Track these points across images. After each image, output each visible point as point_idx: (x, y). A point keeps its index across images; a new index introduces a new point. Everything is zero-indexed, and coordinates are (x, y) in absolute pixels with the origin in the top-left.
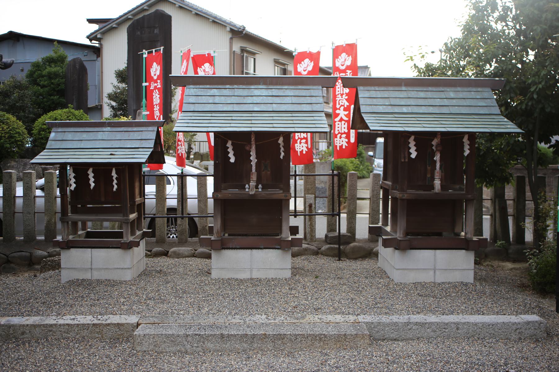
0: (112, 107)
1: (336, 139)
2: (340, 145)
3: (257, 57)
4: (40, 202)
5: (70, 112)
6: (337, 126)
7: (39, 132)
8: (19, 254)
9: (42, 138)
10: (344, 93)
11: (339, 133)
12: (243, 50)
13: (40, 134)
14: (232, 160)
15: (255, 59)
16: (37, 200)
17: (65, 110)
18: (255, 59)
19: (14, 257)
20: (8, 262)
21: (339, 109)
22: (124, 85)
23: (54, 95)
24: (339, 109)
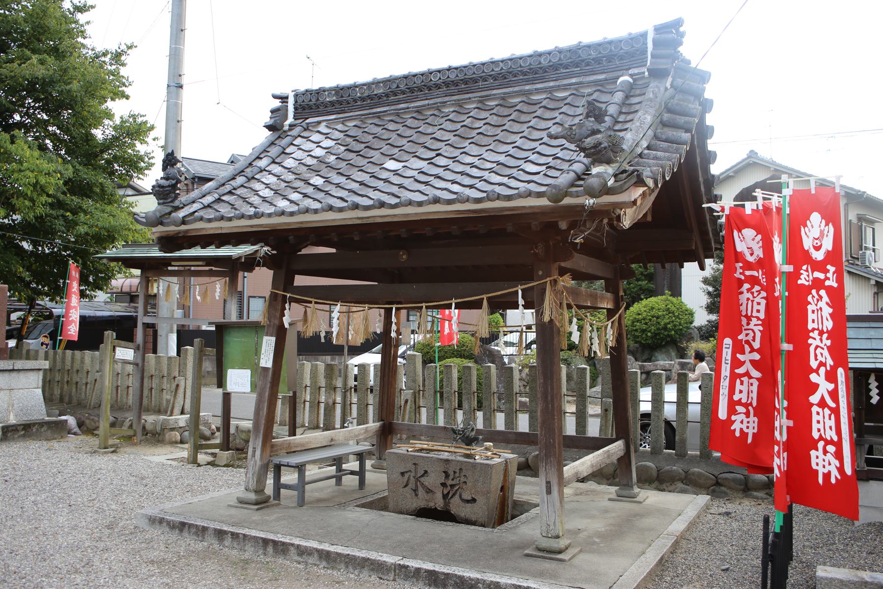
0: (709, 293)
1: (813, 453)
2: (826, 471)
3: (876, 226)
4: (694, 411)
5: (667, 300)
6: (815, 418)
7: (633, 322)
8: (732, 475)
9: (636, 330)
10: (825, 330)
11: (821, 438)
12: (860, 218)
13: (633, 325)
14: (875, 399)
15: (873, 229)
16: (690, 407)
17: (660, 297)
18: (873, 229)
19: (726, 479)
20: (718, 484)
21: (817, 371)
22: (721, 266)
23: (642, 280)
24: (817, 371)
